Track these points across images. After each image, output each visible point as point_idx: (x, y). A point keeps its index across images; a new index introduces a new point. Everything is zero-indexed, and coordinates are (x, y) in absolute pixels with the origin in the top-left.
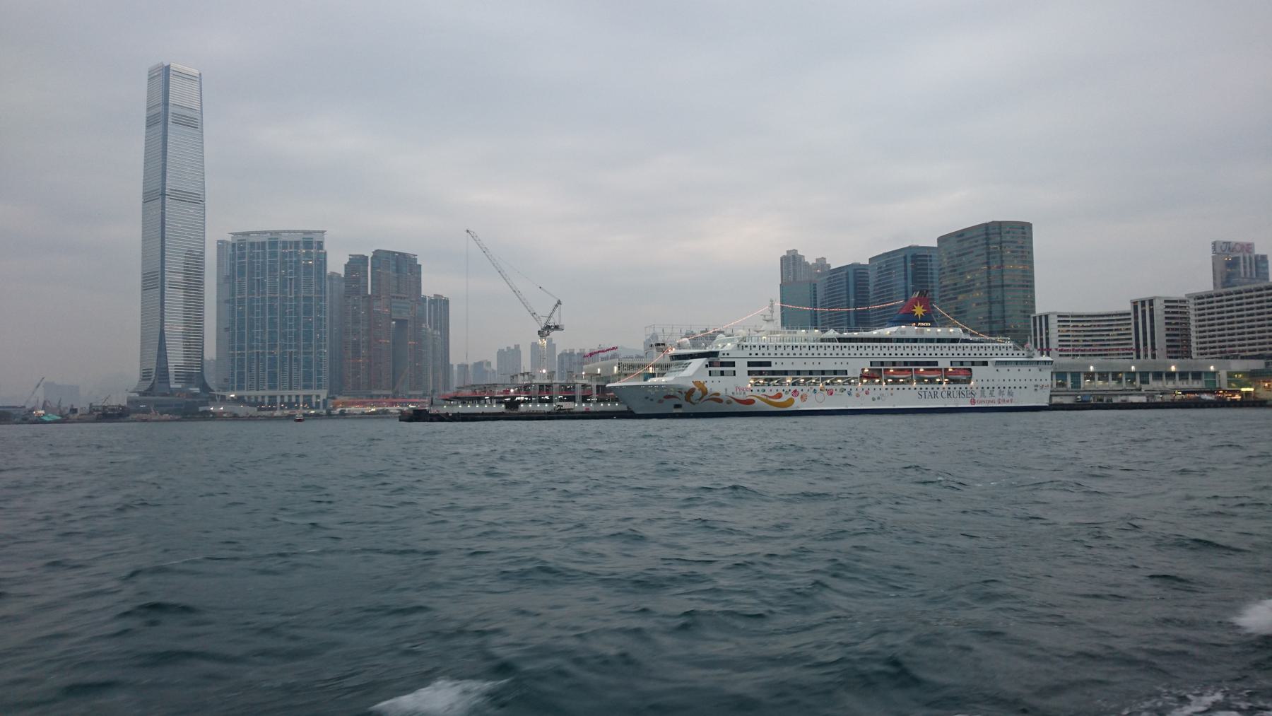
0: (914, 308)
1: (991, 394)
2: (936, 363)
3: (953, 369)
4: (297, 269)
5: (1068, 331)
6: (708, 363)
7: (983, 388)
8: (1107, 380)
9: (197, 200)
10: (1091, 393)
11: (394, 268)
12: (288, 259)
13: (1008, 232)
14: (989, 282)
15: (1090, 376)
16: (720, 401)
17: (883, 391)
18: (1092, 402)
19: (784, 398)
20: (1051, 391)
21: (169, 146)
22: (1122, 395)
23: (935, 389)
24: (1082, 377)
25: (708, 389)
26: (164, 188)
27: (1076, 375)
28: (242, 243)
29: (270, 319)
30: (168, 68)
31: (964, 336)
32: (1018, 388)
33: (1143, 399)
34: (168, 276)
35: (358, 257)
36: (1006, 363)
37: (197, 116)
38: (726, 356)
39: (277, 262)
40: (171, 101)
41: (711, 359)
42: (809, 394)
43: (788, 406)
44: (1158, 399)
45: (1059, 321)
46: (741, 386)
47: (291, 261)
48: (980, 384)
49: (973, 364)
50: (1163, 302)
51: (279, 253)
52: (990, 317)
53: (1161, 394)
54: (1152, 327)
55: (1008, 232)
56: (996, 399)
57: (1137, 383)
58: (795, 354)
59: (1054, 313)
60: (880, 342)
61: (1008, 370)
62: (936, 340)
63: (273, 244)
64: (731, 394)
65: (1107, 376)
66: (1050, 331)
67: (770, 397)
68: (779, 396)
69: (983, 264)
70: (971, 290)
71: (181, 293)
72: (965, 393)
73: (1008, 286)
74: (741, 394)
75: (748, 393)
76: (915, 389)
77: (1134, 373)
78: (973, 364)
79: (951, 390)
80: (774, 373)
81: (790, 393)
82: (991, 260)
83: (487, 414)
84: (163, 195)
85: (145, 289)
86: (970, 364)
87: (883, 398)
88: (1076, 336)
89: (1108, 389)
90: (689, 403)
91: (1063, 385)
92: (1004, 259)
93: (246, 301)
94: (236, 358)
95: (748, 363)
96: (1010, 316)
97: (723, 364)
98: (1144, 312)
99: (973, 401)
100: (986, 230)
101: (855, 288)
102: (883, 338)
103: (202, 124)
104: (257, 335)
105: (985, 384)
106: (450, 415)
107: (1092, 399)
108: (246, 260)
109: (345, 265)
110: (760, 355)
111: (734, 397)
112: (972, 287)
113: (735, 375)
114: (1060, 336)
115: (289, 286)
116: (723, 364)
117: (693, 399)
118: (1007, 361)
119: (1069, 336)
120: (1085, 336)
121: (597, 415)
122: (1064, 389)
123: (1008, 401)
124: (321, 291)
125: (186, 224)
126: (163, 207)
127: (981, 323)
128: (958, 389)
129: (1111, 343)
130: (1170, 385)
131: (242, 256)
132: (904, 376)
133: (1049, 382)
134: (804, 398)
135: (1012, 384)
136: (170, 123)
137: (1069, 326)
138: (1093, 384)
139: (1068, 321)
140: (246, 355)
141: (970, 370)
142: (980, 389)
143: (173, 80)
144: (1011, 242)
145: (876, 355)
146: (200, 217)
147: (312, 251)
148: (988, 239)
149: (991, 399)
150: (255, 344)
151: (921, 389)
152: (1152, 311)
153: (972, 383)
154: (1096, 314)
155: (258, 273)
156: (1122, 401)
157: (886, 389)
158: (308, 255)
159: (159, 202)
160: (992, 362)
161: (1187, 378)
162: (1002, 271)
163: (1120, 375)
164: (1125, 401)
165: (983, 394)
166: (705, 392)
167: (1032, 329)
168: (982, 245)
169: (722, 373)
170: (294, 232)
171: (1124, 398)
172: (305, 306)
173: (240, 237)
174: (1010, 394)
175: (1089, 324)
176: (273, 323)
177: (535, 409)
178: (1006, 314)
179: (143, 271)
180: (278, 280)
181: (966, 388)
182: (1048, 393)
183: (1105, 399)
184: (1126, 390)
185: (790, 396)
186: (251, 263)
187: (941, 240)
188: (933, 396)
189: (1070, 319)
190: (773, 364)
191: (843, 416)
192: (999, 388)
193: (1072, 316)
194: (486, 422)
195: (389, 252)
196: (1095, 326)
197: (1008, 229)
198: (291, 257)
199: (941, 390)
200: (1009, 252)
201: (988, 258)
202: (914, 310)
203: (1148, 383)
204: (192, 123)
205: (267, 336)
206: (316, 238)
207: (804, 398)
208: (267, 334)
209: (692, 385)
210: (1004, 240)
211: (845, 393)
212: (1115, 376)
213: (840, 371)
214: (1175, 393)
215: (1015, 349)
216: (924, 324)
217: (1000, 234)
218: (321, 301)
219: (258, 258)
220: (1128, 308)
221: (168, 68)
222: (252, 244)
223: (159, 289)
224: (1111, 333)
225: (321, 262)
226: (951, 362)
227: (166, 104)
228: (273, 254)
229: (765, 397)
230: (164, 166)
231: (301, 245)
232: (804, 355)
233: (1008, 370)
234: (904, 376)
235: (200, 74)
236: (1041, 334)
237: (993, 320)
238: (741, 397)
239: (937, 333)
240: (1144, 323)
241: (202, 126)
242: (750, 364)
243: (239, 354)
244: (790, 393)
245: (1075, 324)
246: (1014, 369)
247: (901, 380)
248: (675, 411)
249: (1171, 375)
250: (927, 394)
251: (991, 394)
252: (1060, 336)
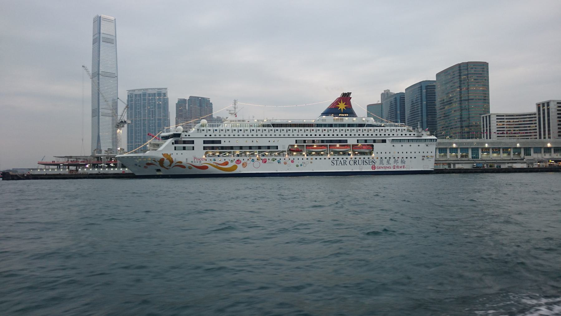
0: (345, 107)
1: (388, 162)
2: (346, 141)
3: (298, 145)
4: (155, 106)
5: (503, 125)
8: (499, 153)
9: (114, 76)
11: (199, 104)
13: (472, 68)
15: (487, 150)
16: (183, 167)
18: (486, 168)
19: (230, 165)
21: (101, 52)
22: (508, 163)
23: (345, 159)
24: (480, 151)
25: (174, 159)
26: (99, 71)
27: (475, 150)
28: (131, 95)
30: (100, 17)
31: (375, 123)
33: (525, 166)
35: (182, 100)
36: (400, 141)
37: (114, 38)
38: (187, 137)
39: (146, 103)
40: (102, 31)
43: (233, 171)
44: (536, 165)
45: (497, 119)
46: (198, 157)
47: (152, 103)
48: (380, 155)
49: (374, 141)
50: (556, 103)
51: (147, 99)
52: (461, 118)
53: (539, 162)
54: (549, 120)
56: (392, 165)
57: (522, 155)
58: (215, 135)
62: (347, 125)
63: (144, 95)
64: (190, 163)
65: (499, 150)
67: (219, 164)
68: (226, 163)
69: (457, 87)
70: (452, 103)
71: (111, 118)
73: (472, 99)
74: (197, 162)
75: (203, 162)
76: (329, 159)
77: (520, 148)
78: (374, 141)
80: (222, 148)
81: (234, 161)
82: (462, 85)
83: (49, 175)
84: (99, 74)
85: (93, 117)
88: (509, 128)
89: (490, 159)
90: (163, 168)
91: (466, 156)
93: (134, 121)
94: (130, 147)
95: (204, 141)
97: (185, 142)
98: (544, 110)
99: (373, 167)
100: (459, 68)
101: (427, 108)
104: (138, 137)
105: (383, 155)
106: (25, 175)
107: (485, 165)
108: (133, 102)
113: (193, 149)
114: (497, 128)
115: (151, 114)
116: (185, 142)
117: (165, 165)
118: (400, 139)
119: (504, 128)
120: (515, 127)
122: (467, 159)
123: (401, 167)
126: (99, 80)
127: (456, 122)
128: (362, 159)
129: (531, 131)
130: (547, 156)
131: (132, 101)
133: (434, 154)
134: (244, 165)
135: (405, 155)
137: (504, 122)
138: (489, 156)
139: (503, 119)
140: (134, 145)
141: (373, 146)
142: (379, 158)
143: (103, 23)
144: (474, 74)
145: (300, 136)
146: (116, 83)
147: (161, 97)
148: (460, 73)
149: (388, 166)
150: (137, 140)
151: (334, 159)
152: (548, 109)
153: (373, 155)
154: (522, 114)
156: (509, 167)
157: (307, 159)
158: (159, 99)
159: (97, 77)
160: (388, 140)
161: (551, 152)
162: (468, 91)
164: (511, 167)
165: (381, 162)
166: (172, 162)
168: (457, 76)
169: (184, 148)
170: (154, 89)
171: (510, 165)
172: (158, 123)
173: (131, 92)
175: (517, 120)
176: (144, 131)
177: (104, 172)
178: (470, 116)
179: (92, 108)
181: (369, 158)
183: (496, 166)
184: (513, 160)
185: (234, 163)
187: (438, 75)
188: (343, 164)
190: (222, 142)
192: (394, 158)
193: (506, 116)
195: (196, 97)
196: (521, 121)
198: (152, 100)
199: (349, 159)
200: (473, 80)
201: (460, 84)
203: (530, 155)
204: (112, 41)
205: (142, 138)
206: (163, 91)
207: (244, 165)
210: (469, 73)
212: (506, 150)
214: (549, 162)
215: (409, 130)
216: (343, 115)
219: (138, 101)
220: (534, 110)
221: (100, 17)
222: (136, 95)
224: (531, 125)
225: (165, 102)
226: (358, 140)
228: (144, 100)
229: (215, 165)
230: (99, 61)
231: (156, 95)
232: (246, 136)
235: (115, 19)
236: (487, 127)
238: (198, 164)
239: (353, 121)
240: (544, 117)
241: (116, 43)
242: (205, 142)
243: (131, 145)
244: (234, 161)
246: (406, 145)
247: (313, 153)
248: (158, 173)
249: (548, 150)
250: (338, 162)
252: (497, 128)
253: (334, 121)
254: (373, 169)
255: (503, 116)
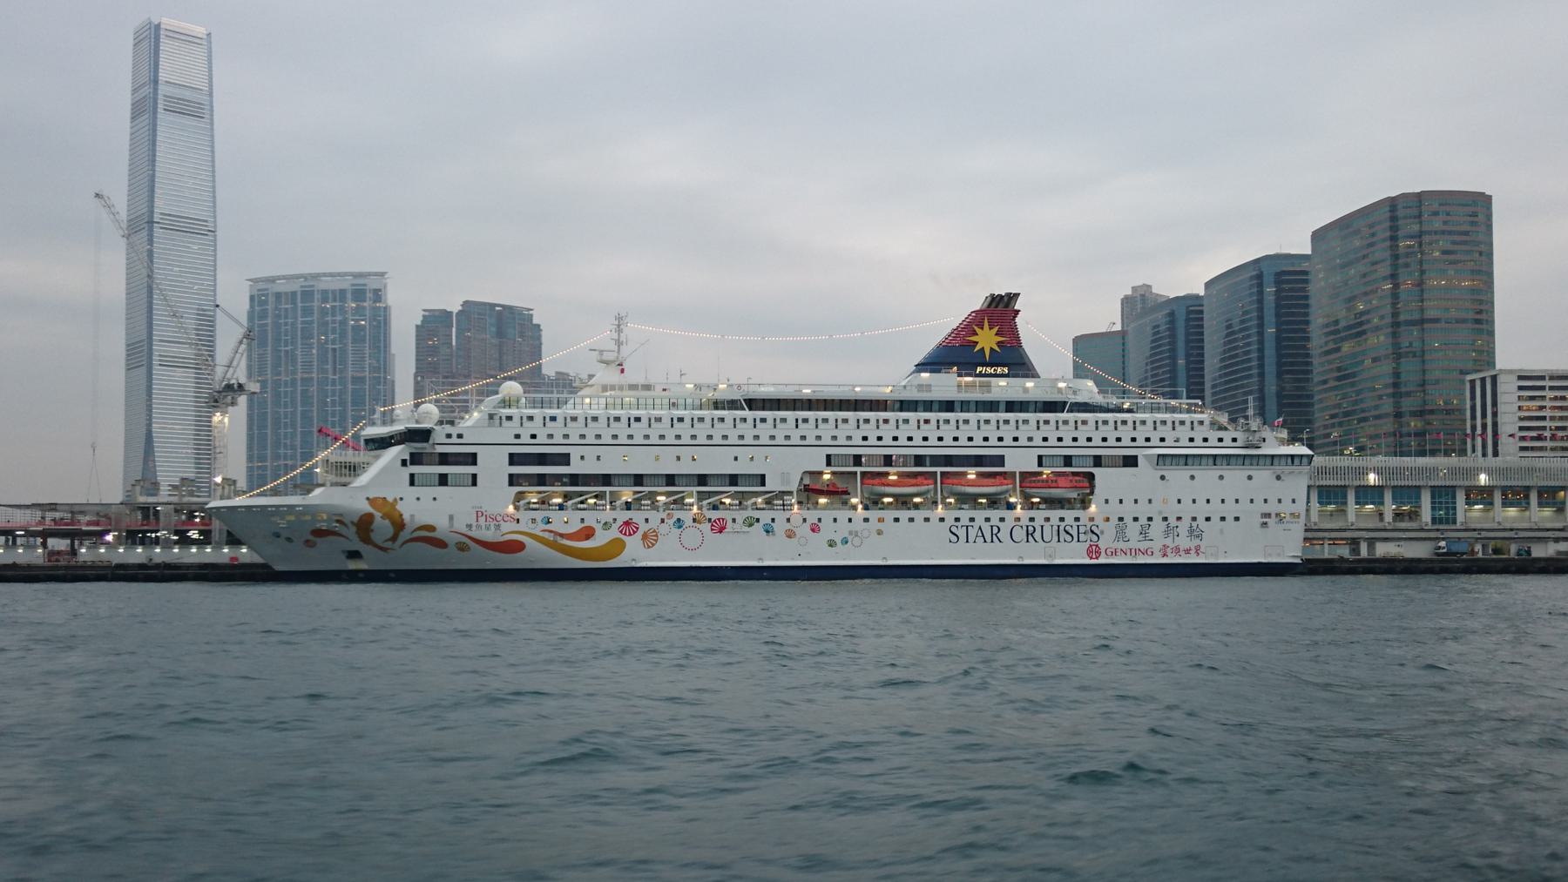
0: (999, 344)
1: (1144, 533)
2: (1000, 460)
4: (343, 335)
5: (1542, 408)
6: (407, 457)
7: (1121, 519)
9: (203, 230)
10: (1475, 534)
11: (494, 329)
12: (329, 318)
13: (1436, 214)
14: (1395, 314)
15: (1483, 495)
16: (441, 544)
17: (858, 524)
18: (1480, 555)
19: (601, 539)
20: (1306, 530)
21: (160, 148)
22: (1557, 540)
23: (995, 521)
25: (406, 517)
28: (263, 295)
29: (303, 413)
30: (158, 27)
31: (1099, 399)
32: (1215, 519)
34: (157, 348)
35: (437, 313)
37: (204, 99)
38: (454, 440)
39: (312, 322)
40: (163, 76)
41: (417, 446)
42: (663, 529)
45: (1521, 388)
46: (490, 509)
47: (334, 322)
48: (1115, 510)
49: (1098, 461)
51: (315, 308)
52: (1396, 385)
55: (1436, 214)
56: (1157, 546)
59: (1511, 372)
60: (855, 410)
61: (1192, 477)
62: (1002, 407)
63: (307, 294)
64: (464, 530)
66: (1501, 408)
67: (562, 535)
68: (588, 533)
69: (1385, 278)
70: (1364, 332)
72: (1075, 533)
73: (1436, 321)
74: (488, 528)
76: (942, 520)
78: (1098, 461)
79: (1037, 524)
80: (575, 479)
81: (615, 527)
84: (151, 222)
85: (129, 368)
86: (1091, 461)
87: (857, 541)
89: (1496, 526)
90: (370, 546)
91: (1414, 515)
92: (1425, 267)
95: (511, 455)
96: (1437, 382)
97: (445, 459)
99: (1093, 551)
101: (1279, 348)
102: (864, 401)
103: (212, 107)
105: (1128, 510)
107: (1478, 547)
108: (269, 321)
109: (417, 326)
110: (541, 439)
111: (470, 533)
112: (1365, 327)
113: (474, 483)
114: (1521, 419)
116: (445, 459)
117: (377, 537)
119: (1544, 418)
121: (1422, 566)
123: (1188, 551)
124: (380, 368)
125: (186, 267)
127: (1380, 397)
128: (1055, 521)
132: (923, 489)
133: (1300, 507)
134: (649, 539)
135: (1201, 510)
136: (160, 110)
137: (1543, 398)
139: (1543, 388)
141: (1091, 476)
142: (1113, 520)
143: (166, 45)
144: (1443, 232)
147: (365, 304)
149: (1143, 545)
150: (282, 451)
151: (957, 520)
153: (1093, 508)
155: (286, 341)
156: (1559, 553)
157: (866, 520)
158: (359, 311)
159: (145, 233)
162: (1422, 291)
163: (1562, 493)
165: (1121, 534)
166: (399, 525)
167: (1468, 406)
168: (1384, 240)
169: (443, 480)
170: (339, 274)
173: (261, 286)
174: (1194, 533)
176: (306, 416)
177: (168, 559)
180: (314, 351)
182: (1298, 530)
183: (1514, 548)
185: (614, 533)
186: (277, 325)
187: (1318, 236)
188: (988, 538)
189: (1548, 383)
190: (574, 459)
191: (582, 585)
192: (1165, 519)
193: (1552, 378)
194: (1109, 579)
195: (485, 304)
197: (1436, 206)
199: (1010, 522)
202: (974, 338)
204: (196, 109)
206: (373, 284)
207: (649, 539)
208: (299, 436)
209: (368, 508)
210: (1425, 228)
211: (758, 527)
213: (741, 475)
216: (990, 370)
217: (1420, 216)
218: (379, 384)
221: (158, 27)
222: (278, 296)
223: (144, 368)
227: (156, 82)
228: (307, 311)
229: (550, 537)
231: (349, 296)
232: (654, 440)
233: (1192, 477)
234: (923, 489)
236: (1484, 415)
237: (1403, 390)
238: (489, 535)
239: (1026, 390)
241: (212, 115)
242: (514, 459)
243: (259, 467)
244: (615, 527)
245: (1559, 394)
247: (887, 500)
248: (353, 565)
250: (973, 532)
251: (1144, 533)
252: (1521, 419)
253: (959, 392)
254: (1091, 558)
255: (1542, 378)
